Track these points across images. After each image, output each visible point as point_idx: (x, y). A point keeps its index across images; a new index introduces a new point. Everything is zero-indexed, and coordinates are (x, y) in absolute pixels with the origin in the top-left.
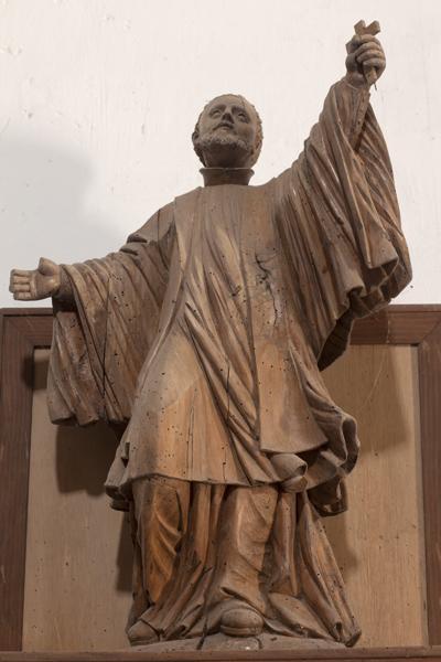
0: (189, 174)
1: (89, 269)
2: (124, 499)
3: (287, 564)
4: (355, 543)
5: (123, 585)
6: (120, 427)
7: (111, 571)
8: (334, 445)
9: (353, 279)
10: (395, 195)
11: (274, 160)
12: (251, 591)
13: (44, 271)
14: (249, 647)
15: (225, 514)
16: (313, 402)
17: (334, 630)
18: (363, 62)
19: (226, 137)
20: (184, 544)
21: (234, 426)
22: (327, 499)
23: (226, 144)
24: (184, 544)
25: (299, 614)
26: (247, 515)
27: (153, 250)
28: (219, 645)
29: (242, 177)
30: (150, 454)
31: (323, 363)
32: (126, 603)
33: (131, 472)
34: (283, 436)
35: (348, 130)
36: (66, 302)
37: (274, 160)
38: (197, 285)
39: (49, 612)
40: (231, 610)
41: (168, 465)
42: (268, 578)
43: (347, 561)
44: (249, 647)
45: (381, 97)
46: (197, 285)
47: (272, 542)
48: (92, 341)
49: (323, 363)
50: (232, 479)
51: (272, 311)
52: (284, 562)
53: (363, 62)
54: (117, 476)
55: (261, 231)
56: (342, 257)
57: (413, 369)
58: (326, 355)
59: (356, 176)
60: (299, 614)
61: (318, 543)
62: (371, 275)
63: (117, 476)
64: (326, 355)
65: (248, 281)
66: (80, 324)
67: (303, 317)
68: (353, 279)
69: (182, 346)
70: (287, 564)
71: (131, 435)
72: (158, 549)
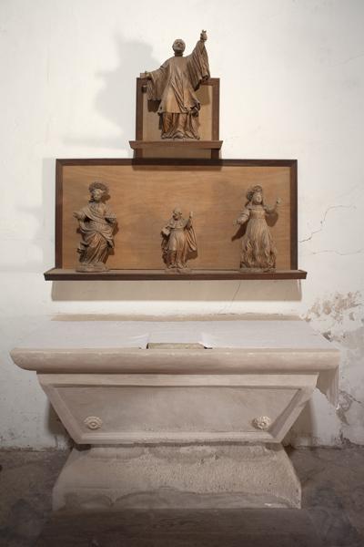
0: (172, 54)
1: (154, 72)
2: (161, 115)
3: (188, 126)
4: (200, 121)
5: (160, 128)
6: (160, 102)
7: (158, 126)
8: (196, 107)
9: (201, 78)
10: (207, 65)
11: (187, 52)
12: (182, 130)
13: (146, 73)
14: (181, 140)
15: (178, 118)
16: (193, 99)
17: (196, 137)
18: (203, 38)
19: (179, 49)
20: (171, 123)
21: (179, 103)
22: (195, 115)
23: (179, 48)
24: (171, 123)
25: (190, 135)
26: (181, 118)
27: (165, 69)
28: (177, 140)
29: (181, 55)
30: (165, 109)
31: (195, 90)
32: (161, 131)
33: (162, 111)
34: (188, 105)
35: (201, 50)
36: (150, 79)
37: (187, 52)
38: (173, 78)
39: (274, 529)
40: (179, 134)
41: (169, 110)
42: (185, 128)
43: (198, 125)
44: (181, 140)
45: (207, 44)
46: (173, 78)
47: (186, 122)
48: (155, 86)
49: (195, 90)
50: (179, 112)
51: (186, 82)
52: (188, 126)
53: (203, 38)
54: (159, 111)
55: (185, 68)
56: (199, 73)
57: (184, 170)
58: (196, 89)
59: (202, 60)
60: (190, 135)
61: (193, 121)
62: (203, 78)
63: (159, 111)
64: (196, 89)
65: (182, 77)
66: (152, 82)
67: (192, 83)
68: (201, 78)
69: (171, 89)
70: (188, 126)
71: (162, 104)
72: (167, 123)
